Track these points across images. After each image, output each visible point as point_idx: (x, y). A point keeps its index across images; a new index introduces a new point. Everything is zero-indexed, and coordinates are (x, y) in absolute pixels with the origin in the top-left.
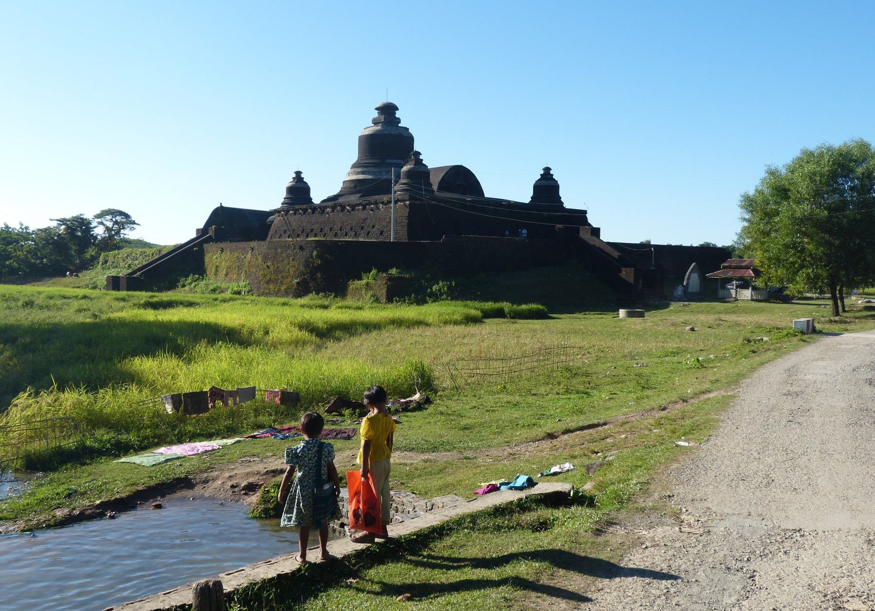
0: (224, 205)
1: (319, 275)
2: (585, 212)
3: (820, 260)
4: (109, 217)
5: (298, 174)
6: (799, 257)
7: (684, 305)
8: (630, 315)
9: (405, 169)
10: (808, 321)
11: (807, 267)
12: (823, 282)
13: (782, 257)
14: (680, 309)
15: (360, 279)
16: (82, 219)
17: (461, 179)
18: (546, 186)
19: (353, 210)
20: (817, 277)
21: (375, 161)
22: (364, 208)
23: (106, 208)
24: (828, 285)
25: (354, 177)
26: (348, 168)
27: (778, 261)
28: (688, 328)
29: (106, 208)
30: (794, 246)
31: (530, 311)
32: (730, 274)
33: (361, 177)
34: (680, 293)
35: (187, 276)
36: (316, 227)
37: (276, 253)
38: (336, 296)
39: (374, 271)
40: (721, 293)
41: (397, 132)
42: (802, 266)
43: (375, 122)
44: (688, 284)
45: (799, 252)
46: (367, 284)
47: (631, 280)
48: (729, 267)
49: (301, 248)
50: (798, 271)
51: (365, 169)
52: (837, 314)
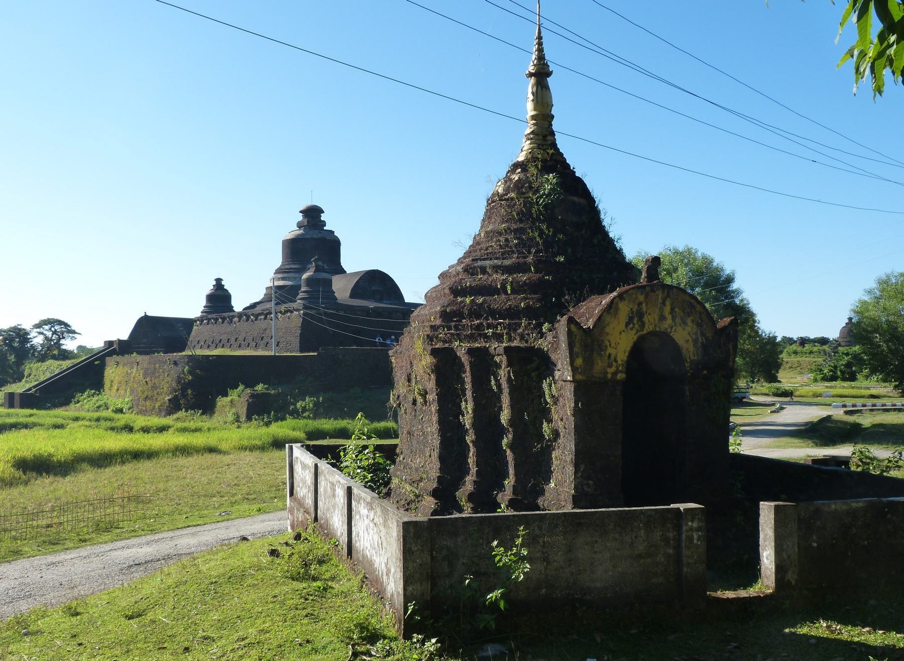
0: (149, 314)
1: (190, 392)
4: (47, 327)
5: (219, 281)
15: (226, 395)
16: (20, 330)
21: (296, 266)
22: (265, 318)
23: (45, 317)
25: (277, 283)
26: (271, 274)
29: (45, 317)
33: (281, 283)
35: (83, 392)
36: (224, 337)
37: (155, 368)
38: (203, 414)
39: (241, 387)
41: (320, 236)
43: (300, 225)
46: (232, 401)
49: (175, 363)
51: (285, 275)
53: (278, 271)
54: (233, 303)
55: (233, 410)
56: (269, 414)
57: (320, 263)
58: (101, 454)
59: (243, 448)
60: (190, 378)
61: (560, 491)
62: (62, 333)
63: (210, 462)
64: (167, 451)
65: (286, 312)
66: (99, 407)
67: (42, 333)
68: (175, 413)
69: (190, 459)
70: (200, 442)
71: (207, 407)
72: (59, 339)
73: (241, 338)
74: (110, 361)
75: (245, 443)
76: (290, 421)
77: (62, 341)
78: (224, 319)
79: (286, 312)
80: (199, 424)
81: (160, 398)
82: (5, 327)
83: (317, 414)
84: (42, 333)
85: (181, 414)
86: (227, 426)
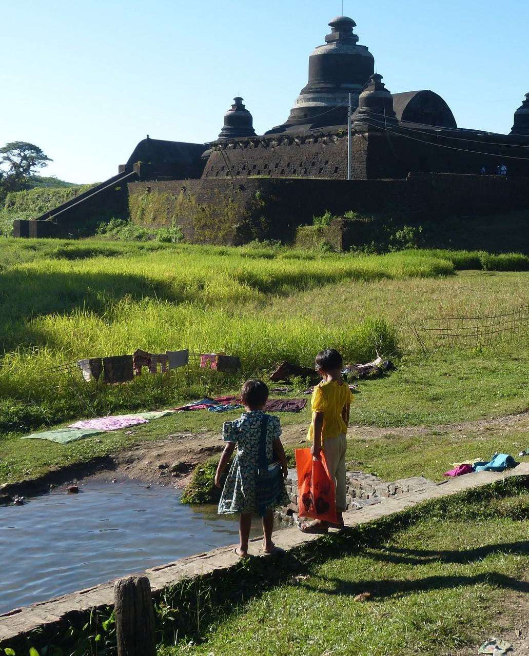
0: (151, 137)
4: (16, 152)
5: (238, 100)
9: (363, 94)
17: (428, 106)
21: (328, 85)
22: (316, 141)
26: (297, 94)
31: (510, 261)
35: (108, 221)
36: (260, 163)
37: (213, 194)
38: (282, 244)
39: (327, 215)
41: (354, 52)
43: (329, 40)
46: (319, 230)
49: (242, 188)
51: (316, 95)
53: (304, 92)
54: (254, 126)
55: (323, 240)
61: (361, 366)
73: (283, 164)
77: (32, 168)
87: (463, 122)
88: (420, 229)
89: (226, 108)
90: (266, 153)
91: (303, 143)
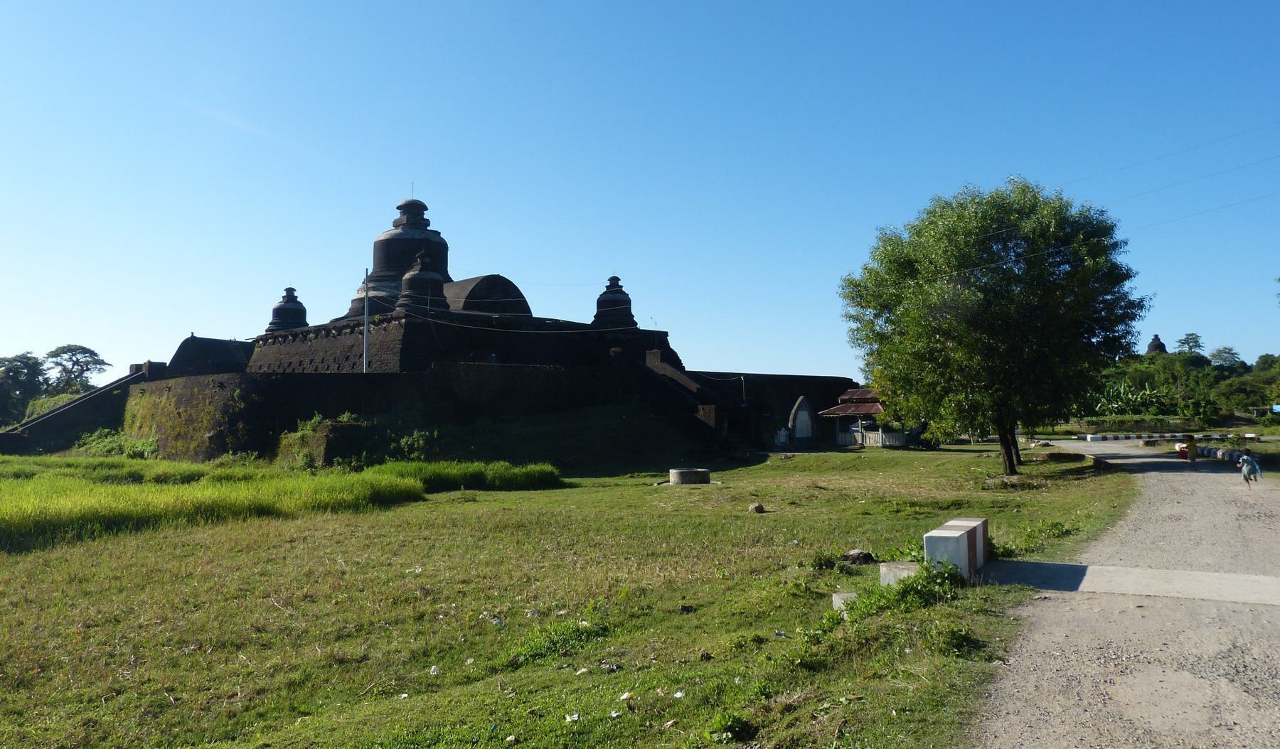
2: (666, 334)
3: (977, 378)
4: (66, 356)
5: (290, 292)
6: (942, 375)
7: (786, 458)
8: (685, 479)
9: (407, 276)
10: (971, 533)
11: (957, 392)
12: (984, 415)
13: (914, 376)
14: (780, 463)
15: (295, 430)
16: (29, 359)
17: (497, 293)
18: (614, 302)
19: (340, 334)
20: (975, 407)
22: (352, 332)
24: (994, 422)
27: (907, 383)
28: (752, 507)
30: (930, 356)
31: (528, 475)
32: (851, 411)
34: (783, 439)
35: (92, 432)
37: (192, 395)
39: (317, 418)
40: (841, 437)
41: (423, 236)
42: (947, 391)
43: (396, 224)
44: (794, 425)
45: (939, 365)
46: (303, 438)
47: (712, 422)
48: (850, 401)
49: (222, 386)
50: (942, 398)
52: (1013, 472)
53: (369, 279)
55: (305, 451)
56: (359, 455)
57: (428, 260)
58: (37, 523)
59: (321, 507)
60: (243, 405)
62: (87, 363)
63: (255, 536)
64: (178, 515)
65: (381, 322)
66: (109, 451)
67: (60, 364)
68: (218, 456)
69: (220, 529)
70: (241, 498)
71: (267, 449)
72: (82, 371)
74: (135, 389)
75: (325, 497)
76: (390, 465)
77: (86, 374)
78: (295, 336)
79: (381, 322)
80: (251, 470)
81: (198, 435)
82: (10, 354)
83: (430, 455)
84: (60, 364)
85: (226, 458)
86: (293, 477)
87: (537, 312)
88: (436, 433)
89: (277, 299)
90: (304, 347)
91: (340, 334)
